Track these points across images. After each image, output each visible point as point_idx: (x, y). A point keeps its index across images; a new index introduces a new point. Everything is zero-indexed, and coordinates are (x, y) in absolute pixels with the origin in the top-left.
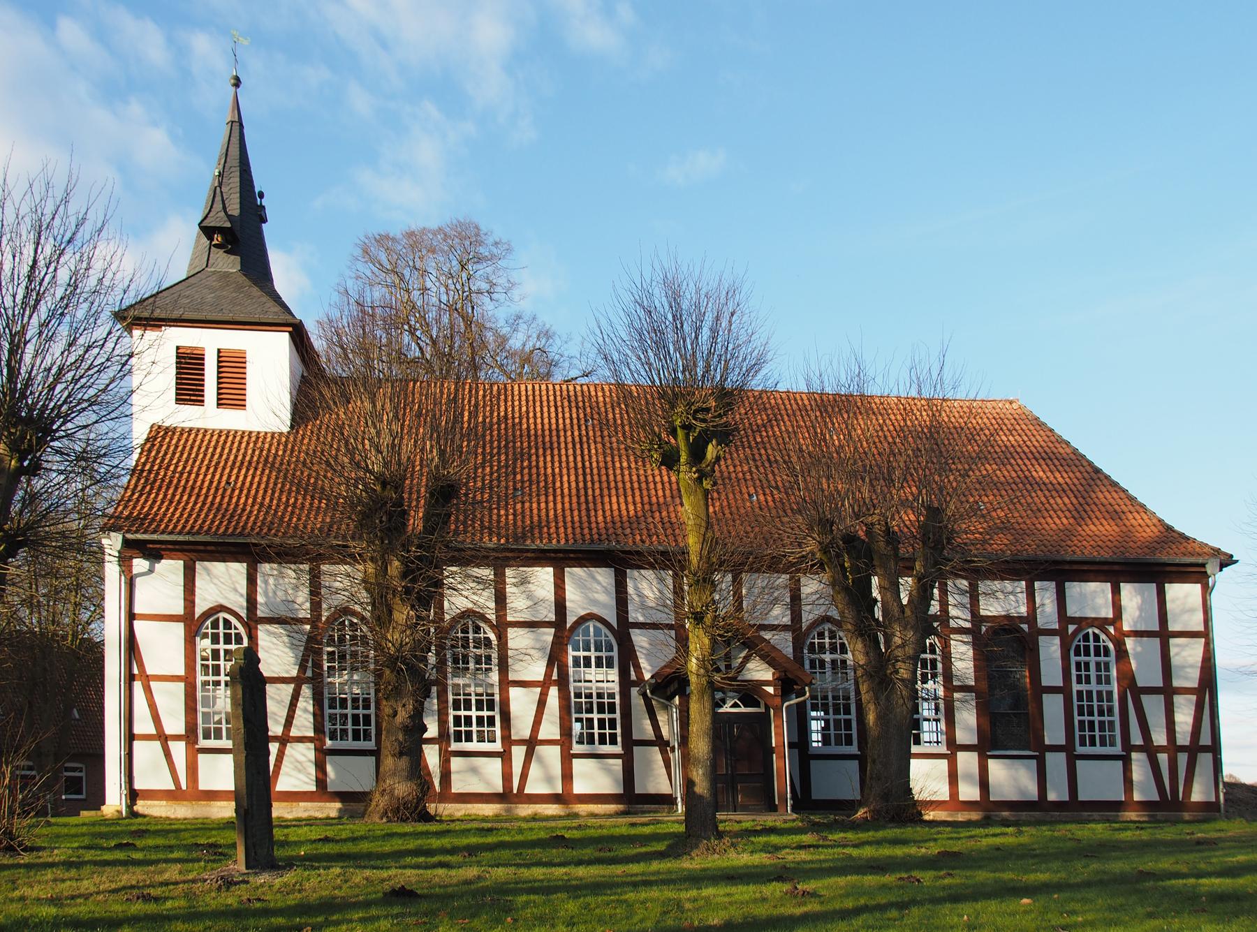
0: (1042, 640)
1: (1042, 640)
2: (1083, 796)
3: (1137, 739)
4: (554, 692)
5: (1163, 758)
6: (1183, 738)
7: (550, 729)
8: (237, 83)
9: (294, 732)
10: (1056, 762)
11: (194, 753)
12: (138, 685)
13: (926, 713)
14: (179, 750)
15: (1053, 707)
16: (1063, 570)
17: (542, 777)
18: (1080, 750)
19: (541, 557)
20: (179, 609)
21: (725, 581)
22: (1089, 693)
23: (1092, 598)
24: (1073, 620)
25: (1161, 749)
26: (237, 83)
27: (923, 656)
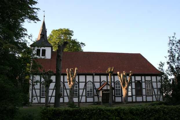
0: (143, 83)
1: (143, 83)
2: (137, 101)
3: (154, 94)
4: (85, 90)
5: (157, 96)
6: (156, 94)
7: (84, 94)
8: (44, 16)
9: (53, 95)
10: (144, 97)
11: (40, 98)
12: (34, 90)
13: (129, 91)
14: (39, 98)
15: (144, 91)
16: (145, 75)
17: (83, 100)
18: (116, 96)
19: (39, 74)
20: (85, 81)
21: (77, 77)
22: (117, 89)
23: (148, 78)
24: (136, 81)
25: (156, 95)
26: (44, 16)
27: (75, 85)
